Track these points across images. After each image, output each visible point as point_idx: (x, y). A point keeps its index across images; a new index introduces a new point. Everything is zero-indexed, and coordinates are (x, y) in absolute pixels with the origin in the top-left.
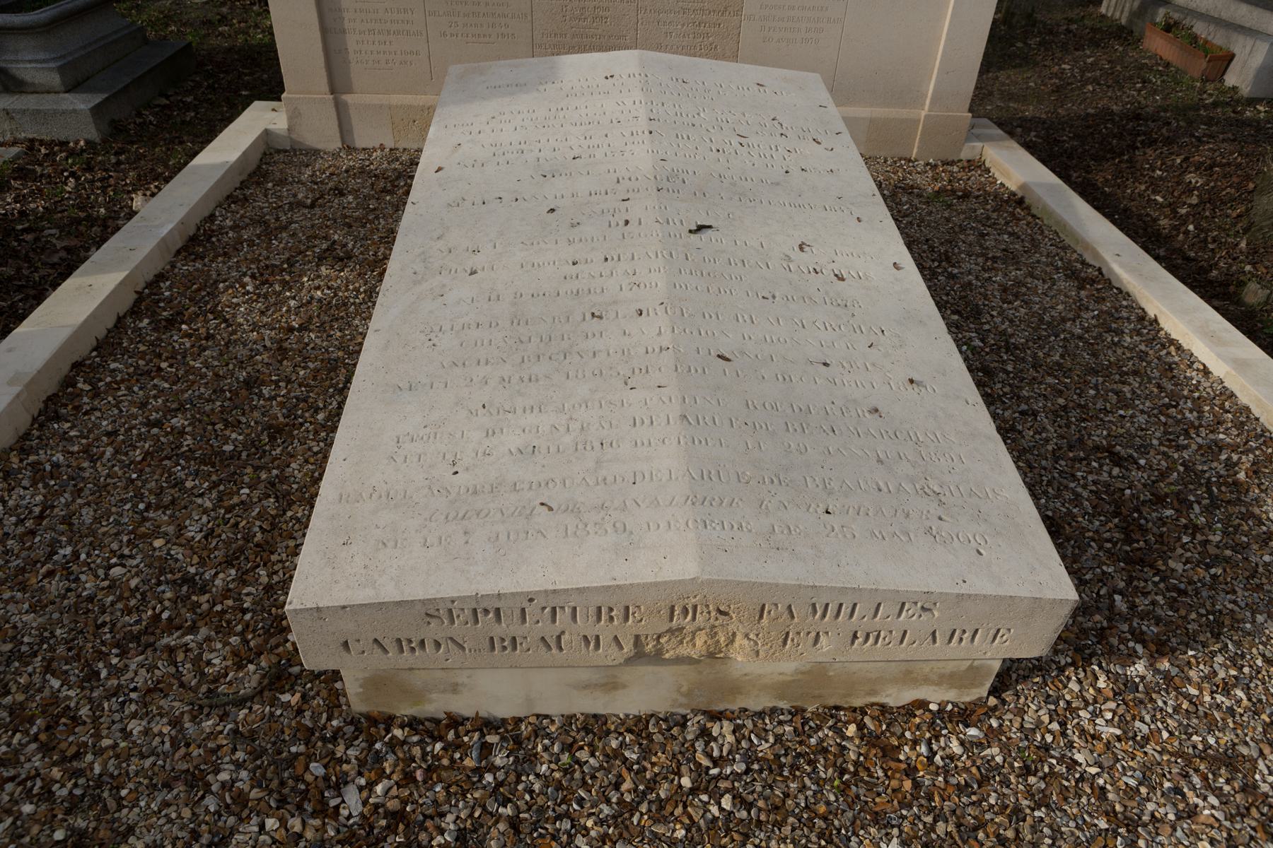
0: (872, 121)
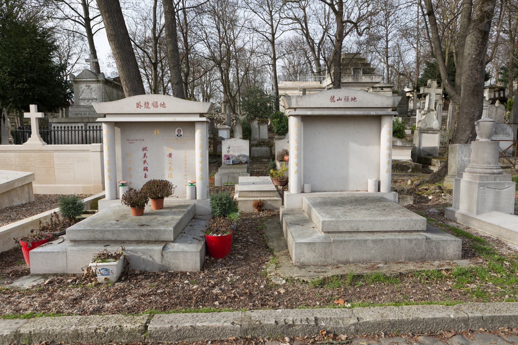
0: (83, 187)
